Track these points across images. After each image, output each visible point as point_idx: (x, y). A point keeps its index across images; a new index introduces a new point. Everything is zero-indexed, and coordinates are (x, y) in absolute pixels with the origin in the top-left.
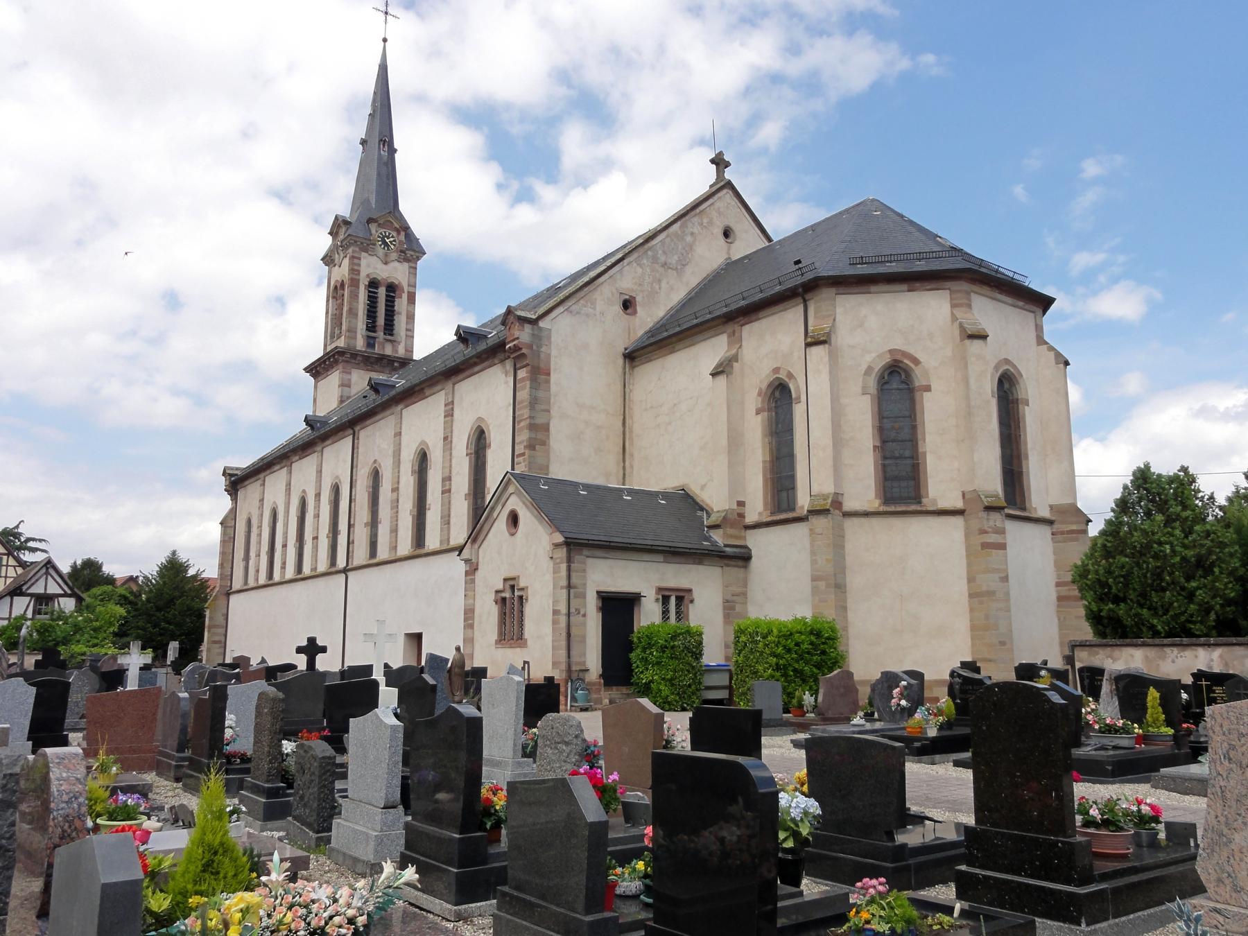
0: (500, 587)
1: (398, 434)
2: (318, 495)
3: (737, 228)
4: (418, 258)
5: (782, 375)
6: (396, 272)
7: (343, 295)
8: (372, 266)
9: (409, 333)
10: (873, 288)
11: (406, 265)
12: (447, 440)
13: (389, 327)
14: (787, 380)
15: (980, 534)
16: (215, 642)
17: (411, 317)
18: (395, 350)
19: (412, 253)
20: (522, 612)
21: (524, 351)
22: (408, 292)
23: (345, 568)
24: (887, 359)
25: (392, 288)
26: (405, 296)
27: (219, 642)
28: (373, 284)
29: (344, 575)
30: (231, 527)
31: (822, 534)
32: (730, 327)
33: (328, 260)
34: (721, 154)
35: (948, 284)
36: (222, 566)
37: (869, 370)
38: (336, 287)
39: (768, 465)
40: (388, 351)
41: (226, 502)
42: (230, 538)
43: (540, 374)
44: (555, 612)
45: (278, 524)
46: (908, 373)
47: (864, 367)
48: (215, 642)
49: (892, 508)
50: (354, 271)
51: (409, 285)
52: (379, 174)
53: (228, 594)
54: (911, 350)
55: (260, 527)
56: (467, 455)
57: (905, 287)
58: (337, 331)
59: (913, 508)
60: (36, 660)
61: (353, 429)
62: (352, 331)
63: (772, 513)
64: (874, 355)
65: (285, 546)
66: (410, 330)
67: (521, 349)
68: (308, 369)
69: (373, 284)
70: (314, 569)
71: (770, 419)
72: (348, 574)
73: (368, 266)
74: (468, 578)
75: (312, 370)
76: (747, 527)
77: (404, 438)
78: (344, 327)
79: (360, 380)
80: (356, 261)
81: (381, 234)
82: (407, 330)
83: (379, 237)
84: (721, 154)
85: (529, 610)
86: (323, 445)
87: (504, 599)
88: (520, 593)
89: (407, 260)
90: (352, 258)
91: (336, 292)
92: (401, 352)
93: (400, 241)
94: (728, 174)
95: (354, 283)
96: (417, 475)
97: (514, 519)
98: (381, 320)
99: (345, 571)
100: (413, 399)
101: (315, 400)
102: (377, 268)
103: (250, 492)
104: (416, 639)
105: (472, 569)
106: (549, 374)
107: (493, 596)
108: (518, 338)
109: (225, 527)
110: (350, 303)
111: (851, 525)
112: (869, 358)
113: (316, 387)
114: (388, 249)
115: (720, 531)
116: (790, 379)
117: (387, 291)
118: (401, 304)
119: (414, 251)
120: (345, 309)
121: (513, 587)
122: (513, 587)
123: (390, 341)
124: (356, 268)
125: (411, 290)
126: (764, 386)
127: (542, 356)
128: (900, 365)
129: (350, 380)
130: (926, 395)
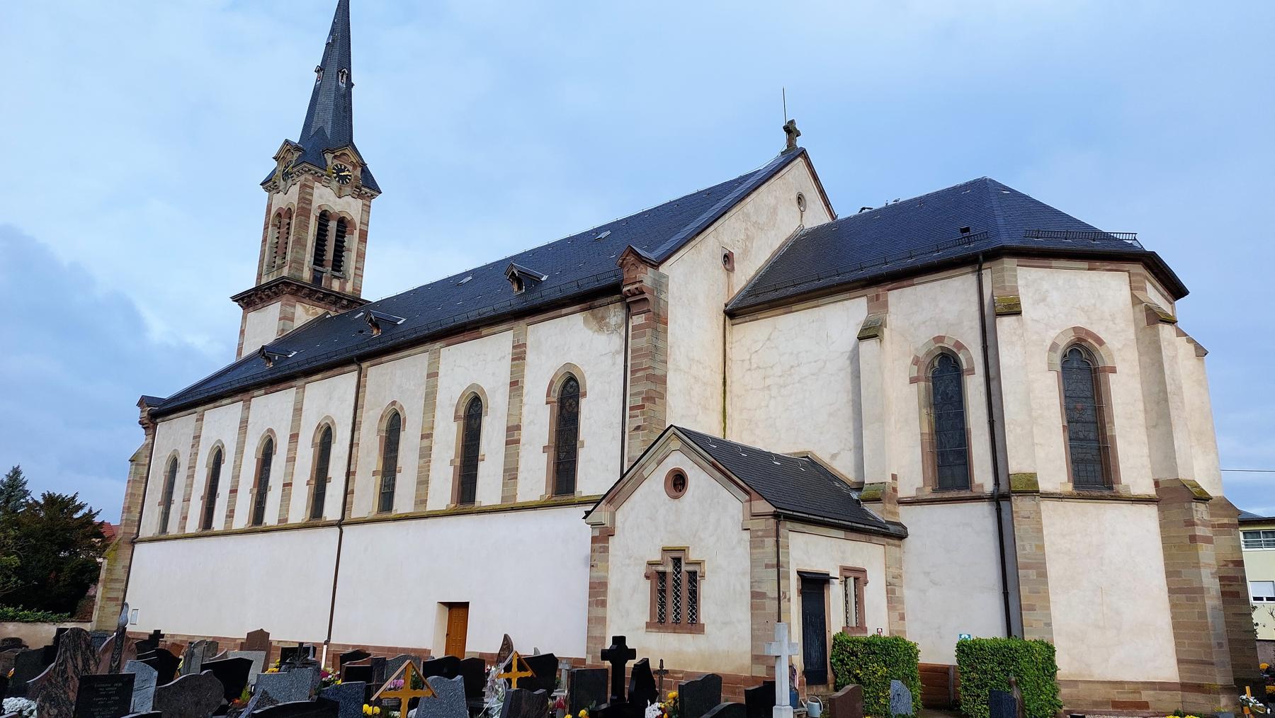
0: (657, 557)
1: (433, 375)
2: (294, 437)
3: (807, 196)
4: (372, 196)
5: (948, 344)
6: (349, 206)
7: (289, 224)
8: (325, 196)
9: (358, 272)
10: (1054, 263)
11: (360, 202)
12: (516, 385)
13: (338, 264)
14: (955, 350)
15: (1186, 526)
16: (110, 599)
17: (361, 256)
18: (343, 286)
19: (368, 190)
20: (695, 592)
21: (646, 296)
22: (360, 229)
23: (340, 521)
24: (1071, 337)
25: (344, 225)
26: (357, 233)
27: (117, 599)
28: (324, 217)
29: (337, 529)
30: (144, 465)
31: (1029, 518)
32: (872, 291)
33: (269, 184)
34: (792, 122)
35: (1128, 266)
36: (127, 509)
37: (1054, 347)
38: (279, 215)
39: (927, 437)
40: (336, 286)
41: (139, 437)
42: (142, 478)
43: (659, 321)
44: (755, 595)
45: (223, 467)
46: (1090, 352)
47: (1048, 343)
48: (110, 599)
49: (946, 495)
50: (305, 200)
51: (361, 223)
52: (336, 105)
53: (134, 542)
54: (1094, 329)
55: (192, 467)
56: (547, 403)
57: (1085, 265)
58: (278, 261)
59: (963, 494)
60: (635, 658)
61: (359, 365)
62: (299, 263)
63: (934, 491)
64: (1058, 331)
65: (234, 491)
66: (359, 269)
67: (643, 293)
68: (236, 299)
69: (324, 217)
70: (283, 520)
71: (927, 388)
72: (344, 528)
73: (321, 197)
74: (597, 545)
75: (242, 299)
76: (902, 502)
77: (443, 381)
78: (288, 257)
79: (304, 314)
80: (308, 190)
81: (337, 166)
82: (356, 268)
83: (334, 169)
84: (792, 122)
85: (706, 589)
86: (306, 380)
87: (662, 576)
88: (691, 568)
89: (360, 196)
90: (303, 186)
91: (280, 220)
92: (349, 288)
93: (356, 176)
94: (800, 142)
95: (305, 212)
96: (461, 422)
97: (678, 482)
98: (329, 255)
99: (340, 524)
100: (461, 338)
101: (242, 332)
102: (329, 200)
103: (175, 431)
104: (457, 611)
105: (603, 536)
106: (666, 324)
107: (643, 569)
108: (642, 281)
109: (137, 465)
110: (297, 232)
111: (1047, 506)
112: (1051, 335)
113: (244, 318)
114: (343, 183)
115: (878, 506)
116: (959, 350)
117: (338, 226)
118: (352, 241)
119: (369, 188)
120: (291, 238)
121: (677, 562)
122: (677, 562)
123: (338, 278)
124: (308, 197)
125: (364, 227)
126: (921, 354)
127: (662, 302)
128: (1083, 344)
129: (294, 313)
130: (1112, 376)
